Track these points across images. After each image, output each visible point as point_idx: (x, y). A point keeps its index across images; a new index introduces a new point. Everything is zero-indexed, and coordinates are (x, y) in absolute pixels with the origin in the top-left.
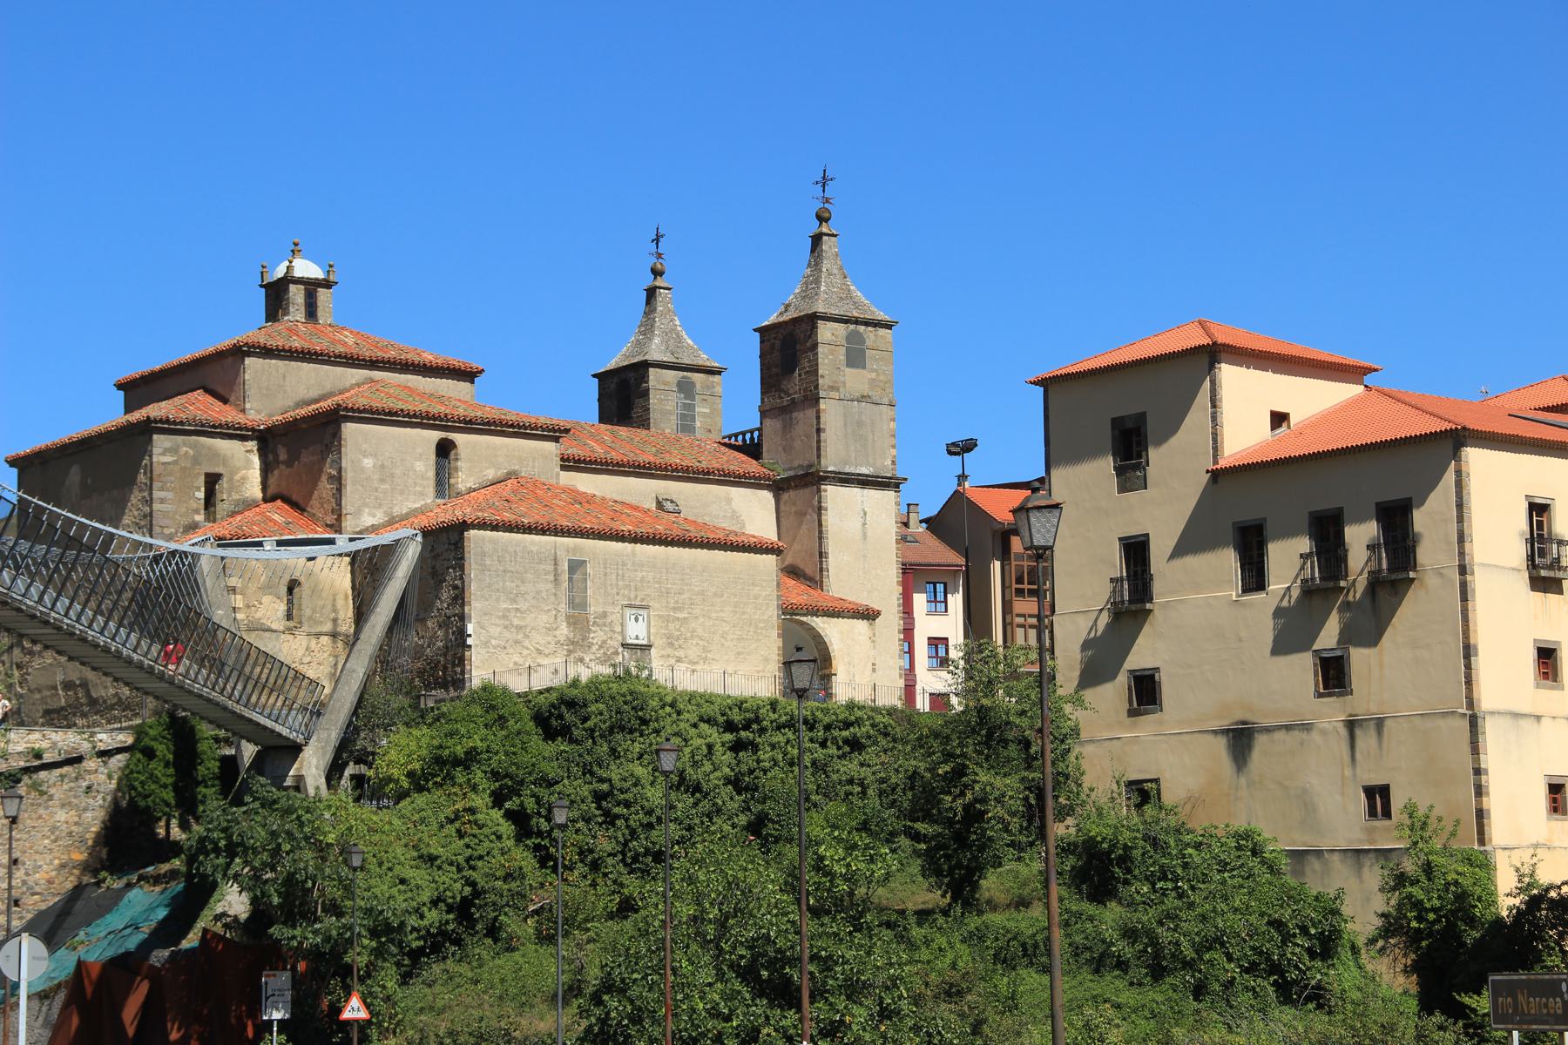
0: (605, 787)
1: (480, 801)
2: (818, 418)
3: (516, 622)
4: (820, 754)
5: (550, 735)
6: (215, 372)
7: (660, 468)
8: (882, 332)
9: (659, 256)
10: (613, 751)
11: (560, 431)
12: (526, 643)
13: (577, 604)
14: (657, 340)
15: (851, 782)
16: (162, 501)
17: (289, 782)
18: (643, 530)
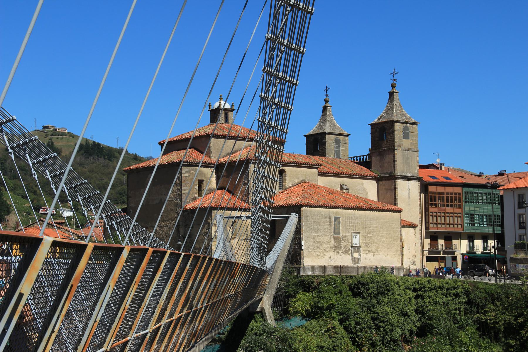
0: (376, 315)
1: (336, 324)
2: (394, 157)
3: (318, 240)
4: (446, 300)
5: (355, 295)
6: (200, 143)
7: (342, 174)
8: (415, 126)
9: (327, 95)
10: (378, 302)
11: (319, 165)
12: (321, 247)
13: (337, 232)
14: (328, 125)
15: (456, 310)
16: (185, 190)
17: (258, 310)
18: (357, 205)
